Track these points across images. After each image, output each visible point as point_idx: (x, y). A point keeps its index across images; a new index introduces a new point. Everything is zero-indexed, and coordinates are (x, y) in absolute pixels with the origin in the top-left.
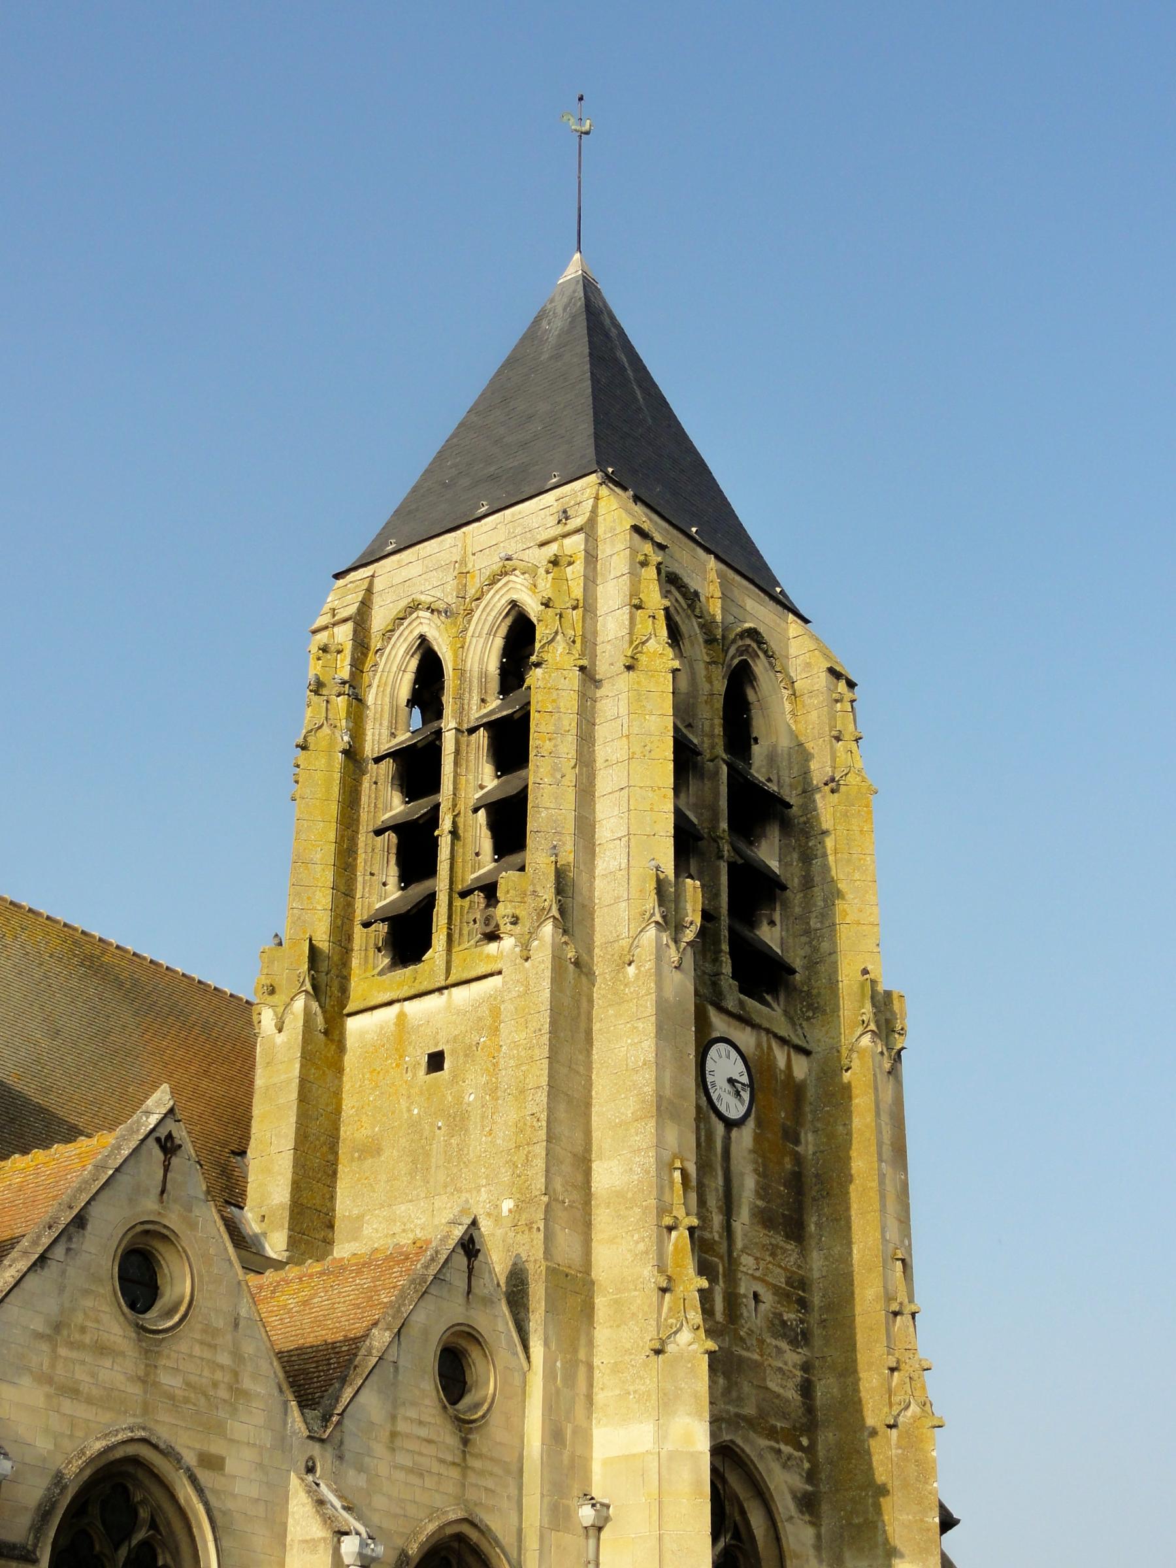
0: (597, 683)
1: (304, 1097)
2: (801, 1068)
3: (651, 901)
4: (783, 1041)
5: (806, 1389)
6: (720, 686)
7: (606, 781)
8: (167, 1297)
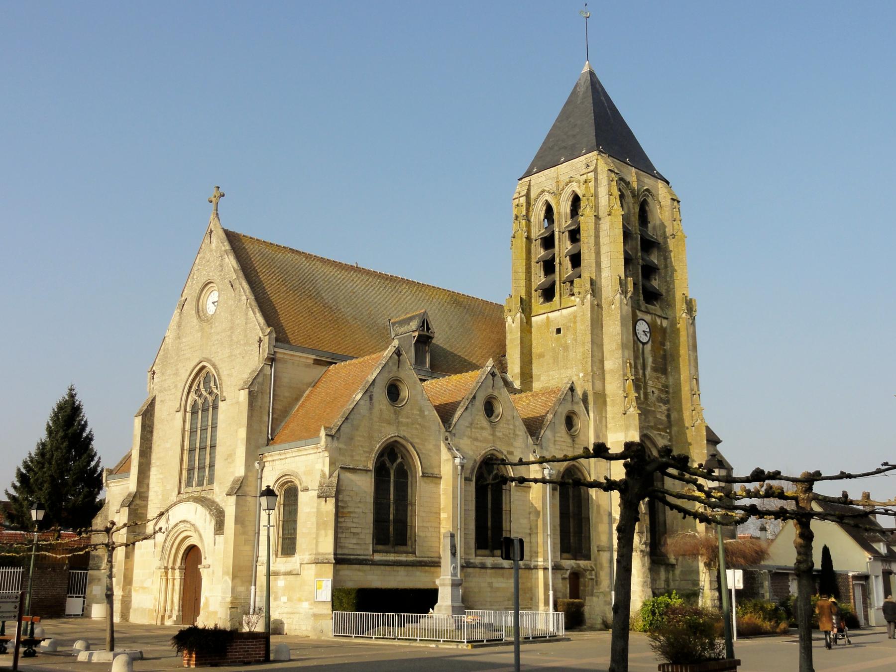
0: (600, 219)
1: (521, 342)
2: (665, 323)
3: (618, 286)
4: (659, 316)
5: (668, 416)
6: (637, 210)
7: (604, 250)
8: (496, 413)
